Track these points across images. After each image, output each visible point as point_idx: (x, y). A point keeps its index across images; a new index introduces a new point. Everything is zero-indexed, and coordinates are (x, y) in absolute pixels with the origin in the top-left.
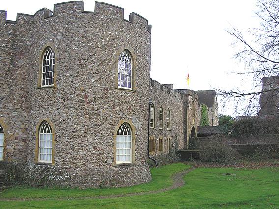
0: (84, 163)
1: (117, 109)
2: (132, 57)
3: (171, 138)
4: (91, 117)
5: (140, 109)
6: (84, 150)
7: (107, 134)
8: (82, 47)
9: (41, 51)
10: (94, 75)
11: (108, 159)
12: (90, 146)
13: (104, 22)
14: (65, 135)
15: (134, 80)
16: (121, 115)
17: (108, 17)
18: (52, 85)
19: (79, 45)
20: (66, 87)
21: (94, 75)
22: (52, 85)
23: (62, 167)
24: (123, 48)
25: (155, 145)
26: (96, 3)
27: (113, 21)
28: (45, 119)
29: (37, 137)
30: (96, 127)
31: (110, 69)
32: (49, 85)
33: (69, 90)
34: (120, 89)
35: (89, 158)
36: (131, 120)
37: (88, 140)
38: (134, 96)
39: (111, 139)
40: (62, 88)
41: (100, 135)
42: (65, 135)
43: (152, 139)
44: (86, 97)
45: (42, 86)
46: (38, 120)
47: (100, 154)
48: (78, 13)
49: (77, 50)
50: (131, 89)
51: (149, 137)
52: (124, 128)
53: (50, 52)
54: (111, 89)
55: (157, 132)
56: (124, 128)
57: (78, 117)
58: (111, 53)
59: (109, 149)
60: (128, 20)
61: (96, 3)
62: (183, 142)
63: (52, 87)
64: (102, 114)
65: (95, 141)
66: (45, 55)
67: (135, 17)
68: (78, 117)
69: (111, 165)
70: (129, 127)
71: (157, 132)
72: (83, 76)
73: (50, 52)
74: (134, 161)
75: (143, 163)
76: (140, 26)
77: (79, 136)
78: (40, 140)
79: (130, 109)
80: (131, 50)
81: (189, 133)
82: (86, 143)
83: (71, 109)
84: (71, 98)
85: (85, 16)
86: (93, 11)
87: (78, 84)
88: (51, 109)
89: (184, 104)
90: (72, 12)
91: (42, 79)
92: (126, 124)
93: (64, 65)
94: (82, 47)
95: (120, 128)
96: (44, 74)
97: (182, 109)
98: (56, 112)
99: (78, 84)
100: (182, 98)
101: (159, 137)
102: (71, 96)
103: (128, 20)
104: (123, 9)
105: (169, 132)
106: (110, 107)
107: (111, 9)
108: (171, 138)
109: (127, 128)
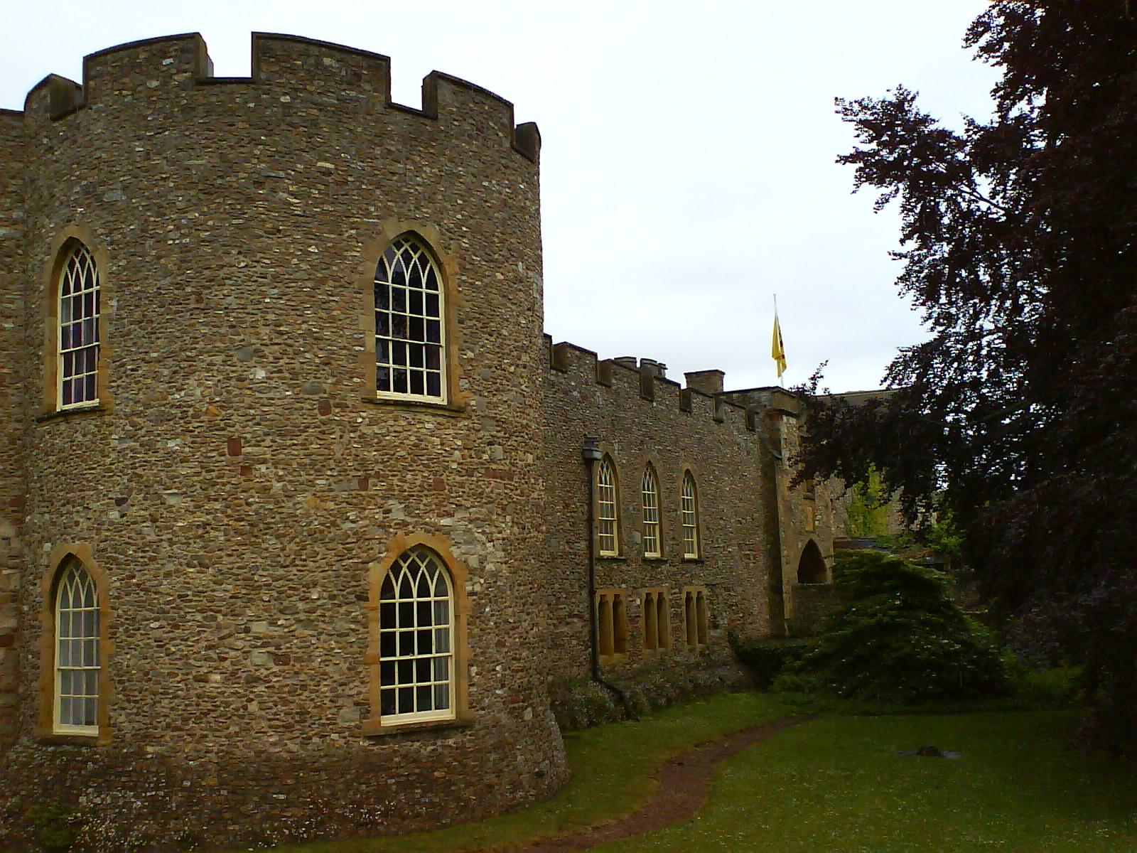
0: (233, 729)
1: (376, 487)
2: (440, 265)
3: (705, 592)
4: (254, 530)
5: (493, 487)
6: (233, 674)
7: (333, 597)
8: (204, 235)
9: (50, 260)
10: (267, 351)
11: (340, 708)
12: (259, 656)
13: (296, 120)
14: (148, 614)
15: (455, 361)
16: (398, 514)
17: (316, 97)
18: (96, 402)
19: (195, 225)
20: (147, 406)
21: (267, 351)
22: (96, 402)
23: (141, 753)
24: (392, 230)
25: (628, 628)
26: (252, 33)
27: (343, 111)
28: (74, 547)
29: (46, 624)
30: (281, 572)
31: (334, 319)
32: (86, 404)
33: (163, 418)
34: (386, 403)
35: (253, 707)
36: (447, 531)
37: (247, 630)
38: (454, 434)
39: (355, 621)
40: (133, 414)
41: (301, 605)
42: (148, 614)
43: (611, 600)
44: (235, 446)
45: (60, 407)
46: (50, 553)
47: (304, 687)
48: (182, 86)
49: (184, 249)
50: (441, 400)
51: (592, 593)
52: (414, 569)
53: (83, 262)
54: (343, 406)
55: (633, 571)
56: (414, 569)
57: (200, 531)
58: (336, 254)
59: (345, 666)
60: (418, 105)
61: (252, 33)
62: (765, 608)
63: (93, 410)
64: (308, 515)
65: (280, 632)
66: (67, 275)
67: (445, 92)
68: (200, 531)
69: (355, 732)
70: (438, 562)
71: (633, 571)
72: (219, 359)
73: (83, 262)
74: (465, 706)
75: (520, 716)
76: (482, 139)
77: (209, 613)
78: (58, 637)
79: (439, 485)
80: (431, 234)
81: (790, 572)
82: (240, 644)
83: (172, 501)
84: (170, 453)
85: (213, 96)
86: (246, 72)
87: (195, 390)
88: (94, 506)
89: (764, 452)
90: (155, 84)
91: (61, 378)
92: (422, 550)
93: (137, 315)
94: (204, 235)
95: (396, 568)
96: (67, 357)
97: (752, 472)
98: (114, 515)
99: (198, 392)
100: (751, 427)
101: (644, 592)
102: (171, 444)
103: (418, 105)
104: (387, 60)
105: (695, 569)
106: (345, 485)
107: (327, 61)
108: (705, 592)
109: (431, 568)
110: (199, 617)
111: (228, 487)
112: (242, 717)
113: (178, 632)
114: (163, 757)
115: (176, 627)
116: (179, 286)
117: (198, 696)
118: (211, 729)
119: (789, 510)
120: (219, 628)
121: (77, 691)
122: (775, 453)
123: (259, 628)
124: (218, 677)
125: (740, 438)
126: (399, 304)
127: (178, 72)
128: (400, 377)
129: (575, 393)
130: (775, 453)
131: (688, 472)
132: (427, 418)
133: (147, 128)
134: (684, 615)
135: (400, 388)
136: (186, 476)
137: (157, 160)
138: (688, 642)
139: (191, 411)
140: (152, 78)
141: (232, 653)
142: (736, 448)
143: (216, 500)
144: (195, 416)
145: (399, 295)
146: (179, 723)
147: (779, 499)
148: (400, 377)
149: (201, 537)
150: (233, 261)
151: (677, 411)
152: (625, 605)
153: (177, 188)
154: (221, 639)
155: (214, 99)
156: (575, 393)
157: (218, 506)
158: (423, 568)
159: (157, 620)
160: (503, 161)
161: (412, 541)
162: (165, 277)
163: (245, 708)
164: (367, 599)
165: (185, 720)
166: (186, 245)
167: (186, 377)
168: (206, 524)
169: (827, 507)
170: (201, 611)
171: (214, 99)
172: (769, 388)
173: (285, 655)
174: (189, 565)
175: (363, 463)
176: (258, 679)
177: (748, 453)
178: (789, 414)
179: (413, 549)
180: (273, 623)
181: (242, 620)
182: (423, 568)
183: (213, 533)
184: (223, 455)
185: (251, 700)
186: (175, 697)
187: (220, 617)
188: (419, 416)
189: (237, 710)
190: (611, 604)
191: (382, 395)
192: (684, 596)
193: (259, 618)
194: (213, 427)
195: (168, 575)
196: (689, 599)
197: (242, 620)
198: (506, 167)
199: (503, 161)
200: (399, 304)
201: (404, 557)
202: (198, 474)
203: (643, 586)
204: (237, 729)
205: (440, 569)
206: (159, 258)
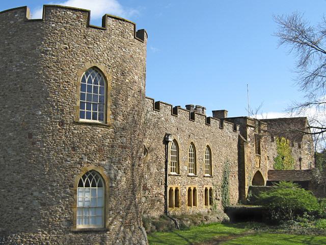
8: (24, 68)
12: (36, 202)
19: (21, 66)
37: (32, 194)
44: (30, 136)
48: (21, 23)
49: (18, 73)
68: (18, 162)
70: (99, 176)
81: (248, 183)
82: (29, 198)
84: (10, 137)
87: (18, 118)
95: (84, 177)
99: (19, 118)
102: (10, 134)
110: (16, 189)
111: (27, 149)
112: (30, 221)
113: (10, 193)
114: (4, 231)
115: (9, 191)
116: (15, 84)
117: (16, 214)
118: (19, 224)
119: (250, 160)
120: (23, 192)
121: (174, 155)
122: (245, 140)
123: (36, 194)
124: (22, 208)
125: (230, 135)
126: (89, 90)
127: (20, 18)
128: (95, 114)
129: (163, 119)
130: (245, 140)
131: (208, 146)
132: (97, 128)
133: (9, 36)
134: (204, 195)
135: (88, 118)
136: (15, 144)
137: (11, 46)
138: (205, 205)
139: (17, 124)
140: (11, 20)
141: (27, 201)
142: (228, 138)
143: (23, 152)
144: (18, 126)
145: (90, 87)
146: (9, 221)
147: (245, 156)
148: (89, 114)
149: (18, 164)
150: (33, 77)
151: (204, 125)
152: (180, 191)
153: (17, 54)
154: (24, 196)
155: (30, 26)
156: (163, 119)
157: (24, 155)
158: (94, 177)
159: (4, 189)
160: (131, 43)
161: (89, 169)
162: (11, 82)
163: (30, 219)
164: (73, 187)
165: (11, 221)
166: (18, 72)
167: (16, 113)
168: (20, 160)
169: (266, 159)
170: (18, 187)
171: (30, 26)
172: (242, 117)
173: (45, 203)
174: (14, 172)
175: (73, 143)
176: (35, 210)
177: (234, 140)
178: (251, 126)
179: (90, 171)
180: (40, 192)
181: (30, 191)
182: (94, 177)
183: (22, 163)
184: (26, 138)
185: (32, 217)
186: (8, 213)
187: (23, 190)
188: (94, 127)
189: (28, 219)
190: (174, 191)
191: (81, 120)
192: (204, 189)
193: (36, 191)
194: (24, 129)
195: (7, 175)
196: (206, 190)
197: (30, 191)
198: (132, 44)
199: (131, 43)
200: (89, 90)
201: (87, 173)
202: (18, 144)
203: (187, 185)
204: (28, 225)
205: (100, 178)
206: (10, 75)
